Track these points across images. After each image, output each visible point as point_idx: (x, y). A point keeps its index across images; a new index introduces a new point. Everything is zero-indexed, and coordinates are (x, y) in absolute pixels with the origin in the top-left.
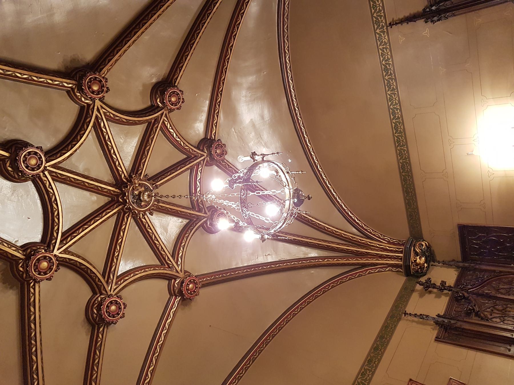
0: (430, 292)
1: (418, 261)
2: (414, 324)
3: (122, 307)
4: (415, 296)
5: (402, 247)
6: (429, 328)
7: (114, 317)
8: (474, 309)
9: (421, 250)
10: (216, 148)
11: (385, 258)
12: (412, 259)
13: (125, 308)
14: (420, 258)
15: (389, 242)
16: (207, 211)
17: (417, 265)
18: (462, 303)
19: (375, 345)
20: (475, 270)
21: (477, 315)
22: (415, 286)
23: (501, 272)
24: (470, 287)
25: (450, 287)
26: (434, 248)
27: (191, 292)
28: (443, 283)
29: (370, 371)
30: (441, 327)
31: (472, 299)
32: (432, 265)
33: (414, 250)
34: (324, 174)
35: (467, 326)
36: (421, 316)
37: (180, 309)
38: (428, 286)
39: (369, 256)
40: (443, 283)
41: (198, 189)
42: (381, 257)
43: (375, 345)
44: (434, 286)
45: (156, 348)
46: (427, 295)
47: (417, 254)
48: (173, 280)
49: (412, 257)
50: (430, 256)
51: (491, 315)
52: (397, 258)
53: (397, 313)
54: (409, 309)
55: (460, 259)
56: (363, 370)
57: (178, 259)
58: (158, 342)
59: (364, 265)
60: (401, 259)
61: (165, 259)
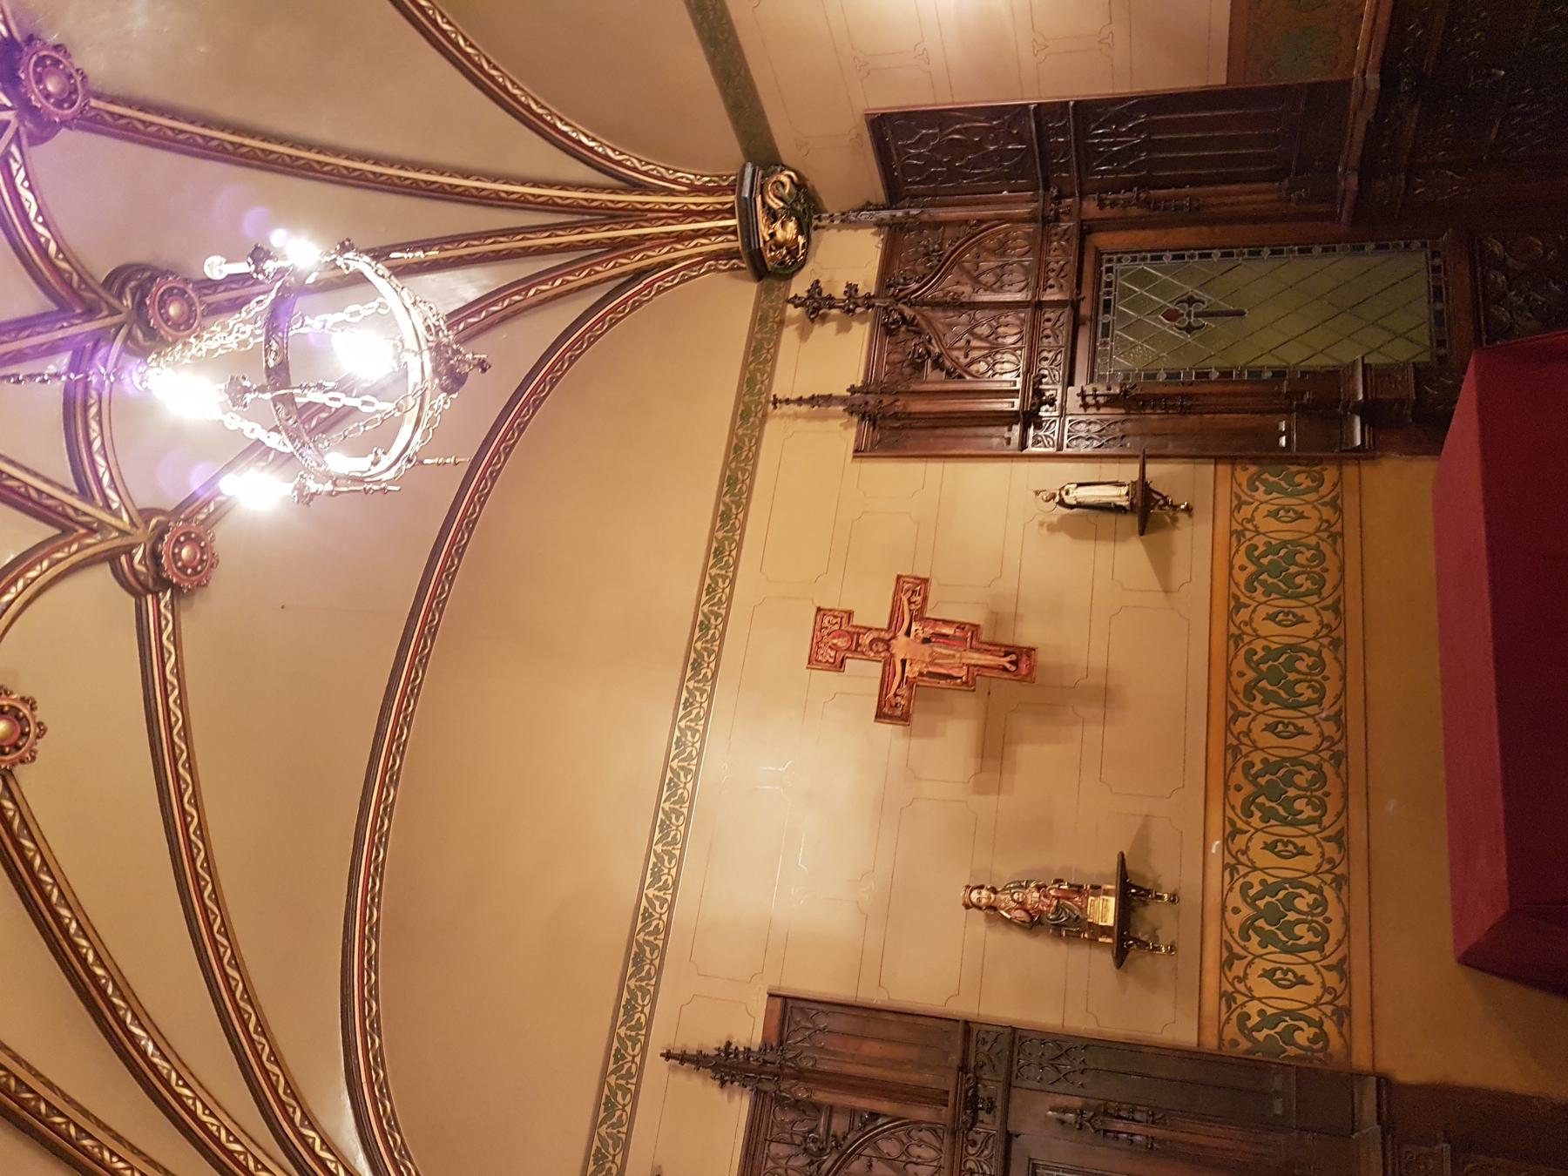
0: (824, 319)
1: (780, 235)
2: (801, 423)
3: (25, 710)
4: (789, 335)
5: (732, 198)
6: (835, 424)
7: (18, 748)
8: (929, 353)
9: (781, 199)
10: (39, 80)
11: (692, 238)
12: (764, 232)
13: (33, 709)
14: (783, 225)
15: (694, 190)
16: (115, 302)
17: (779, 246)
18: (902, 336)
19: (722, 507)
20: (922, 225)
21: (938, 364)
22: (783, 310)
23: (980, 221)
24: (914, 286)
25: (868, 297)
26: (816, 181)
27: (194, 569)
28: (851, 289)
29: (724, 578)
30: (863, 418)
31: (923, 324)
32: (816, 228)
33: (764, 203)
34: (443, 16)
35: (919, 406)
36: (813, 400)
37: (183, 615)
38: (817, 306)
39: (648, 244)
40: (851, 289)
41: (52, 248)
42: (681, 237)
43: (722, 507)
44: (830, 301)
45: (172, 744)
46: (817, 327)
47: (773, 216)
48: (123, 559)
49: (762, 227)
50: (807, 208)
51: (966, 356)
52: (724, 231)
53: (754, 407)
54: (782, 386)
55: (880, 195)
56: (708, 581)
57: (105, 497)
58: (170, 729)
59: (639, 274)
60: (734, 233)
61: (66, 516)
